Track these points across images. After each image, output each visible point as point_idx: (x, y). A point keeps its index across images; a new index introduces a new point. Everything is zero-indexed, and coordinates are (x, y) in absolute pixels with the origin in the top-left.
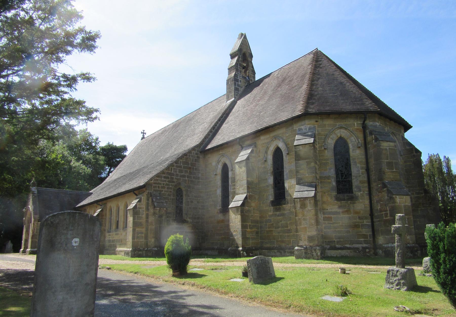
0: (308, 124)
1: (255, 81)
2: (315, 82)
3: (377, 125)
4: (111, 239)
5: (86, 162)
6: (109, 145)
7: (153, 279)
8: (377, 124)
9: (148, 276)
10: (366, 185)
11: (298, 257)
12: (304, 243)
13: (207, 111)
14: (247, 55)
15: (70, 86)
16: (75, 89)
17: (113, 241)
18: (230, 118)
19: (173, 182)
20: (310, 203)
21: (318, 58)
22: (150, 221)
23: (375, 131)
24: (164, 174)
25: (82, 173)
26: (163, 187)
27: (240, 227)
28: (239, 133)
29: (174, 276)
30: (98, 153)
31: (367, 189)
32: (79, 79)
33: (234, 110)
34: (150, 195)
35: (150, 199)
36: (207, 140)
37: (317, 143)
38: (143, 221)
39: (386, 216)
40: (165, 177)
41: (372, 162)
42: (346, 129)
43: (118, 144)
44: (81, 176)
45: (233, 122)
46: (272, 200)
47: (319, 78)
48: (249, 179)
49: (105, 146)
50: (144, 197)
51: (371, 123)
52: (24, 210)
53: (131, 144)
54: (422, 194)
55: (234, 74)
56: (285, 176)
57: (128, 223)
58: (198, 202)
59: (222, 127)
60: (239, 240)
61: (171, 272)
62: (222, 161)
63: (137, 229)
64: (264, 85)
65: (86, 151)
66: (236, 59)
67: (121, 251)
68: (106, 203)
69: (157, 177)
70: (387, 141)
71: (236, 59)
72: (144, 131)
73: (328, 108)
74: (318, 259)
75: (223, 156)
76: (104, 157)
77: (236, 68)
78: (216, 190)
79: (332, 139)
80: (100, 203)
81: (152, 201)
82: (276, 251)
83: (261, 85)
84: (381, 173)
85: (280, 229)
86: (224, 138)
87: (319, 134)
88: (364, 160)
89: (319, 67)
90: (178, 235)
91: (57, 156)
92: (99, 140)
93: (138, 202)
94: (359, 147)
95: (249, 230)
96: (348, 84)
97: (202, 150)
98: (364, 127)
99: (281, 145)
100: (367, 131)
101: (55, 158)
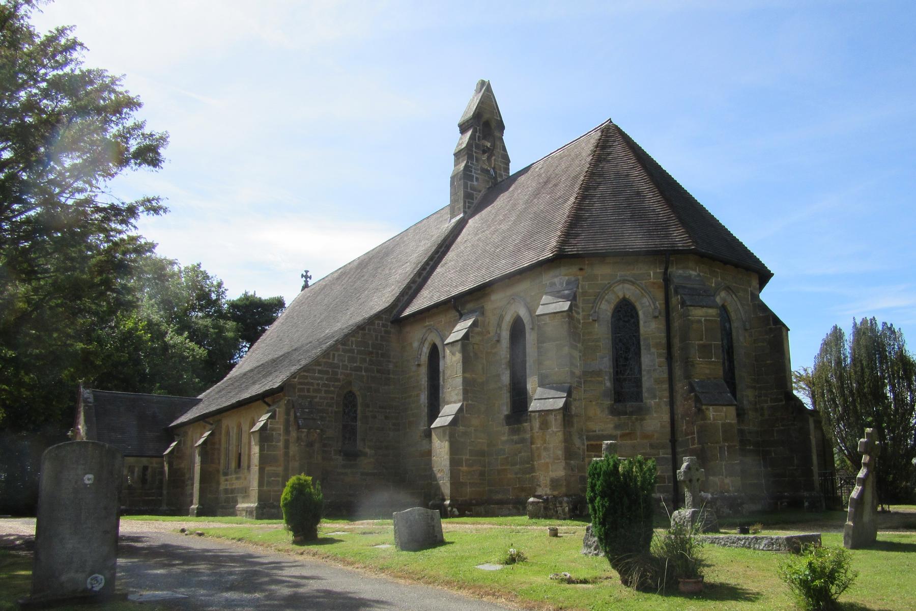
0: (566, 275)
1: (510, 177)
2: (592, 192)
3: (690, 275)
4: (228, 487)
5: (197, 336)
6: (246, 297)
7: (261, 548)
8: (693, 273)
9: (256, 544)
10: (666, 386)
11: (533, 516)
12: (545, 490)
13: (417, 237)
14: (493, 124)
15: (124, 222)
16: (135, 227)
17: (232, 491)
18: (451, 255)
19: (338, 380)
20: (556, 420)
21: (608, 141)
22: (291, 453)
23: (685, 287)
24: (320, 365)
25: (188, 357)
26: (318, 391)
27: (448, 463)
28: (456, 286)
29: (295, 542)
30: (221, 315)
31: (666, 394)
32: (141, 208)
33: (459, 239)
34: (291, 406)
35: (292, 413)
36: (406, 298)
37: (580, 310)
38: (280, 452)
39: (693, 444)
40: (320, 372)
41: (676, 342)
42: (633, 283)
43: (265, 294)
44: (187, 363)
45: (453, 263)
46: (506, 413)
47: (600, 184)
48: (467, 375)
49: (239, 300)
50: (280, 410)
51: (680, 272)
52: (70, 433)
53: (290, 294)
54: (781, 401)
55: (463, 165)
56: (528, 371)
57: (252, 456)
58: (386, 418)
59: (435, 273)
60: (445, 486)
61: (290, 536)
62: (429, 339)
63: (268, 469)
64: (516, 189)
65: (201, 310)
66: (469, 134)
67: (243, 509)
68: (220, 420)
69: (305, 371)
70: (703, 307)
71: (469, 134)
72: (307, 272)
73: (601, 245)
74: (565, 519)
75: (430, 329)
76: (235, 323)
77: (468, 153)
78: (418, 395)
79: (608, 302)
80: (211, 420)
81: (296, 417)
82: (510, 506)
83: (511, 189)
84: (688, 364)
85: (518, 466)
86: (432, 297)
87: (584, 294)
88: (664, 341)
89: (604, 159)
90: (303, 476)
91: (136, 324)
92: (225, 286)
93: (269, 418)
94: (656, 317)
95: (464, 468)
96: (650, 195)
97: (394, 319)
98: (667, 280)
99: (523, 313)
100: (672, 287)
101: (132, 329)
